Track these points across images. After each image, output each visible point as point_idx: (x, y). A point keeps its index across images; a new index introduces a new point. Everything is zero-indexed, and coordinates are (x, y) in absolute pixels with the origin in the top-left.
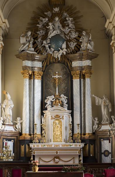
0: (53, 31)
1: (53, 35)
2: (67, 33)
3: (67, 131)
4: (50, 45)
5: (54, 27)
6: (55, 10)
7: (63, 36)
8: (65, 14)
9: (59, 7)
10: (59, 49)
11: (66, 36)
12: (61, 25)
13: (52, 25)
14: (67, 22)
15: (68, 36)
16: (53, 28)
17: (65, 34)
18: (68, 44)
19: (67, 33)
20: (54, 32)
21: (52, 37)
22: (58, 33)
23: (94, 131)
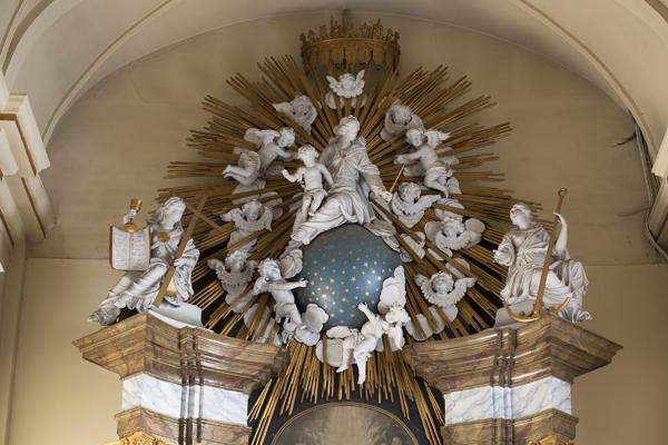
0: (324, 201)
1: (327, 227)
4: (302, 284)
6: (340, 93)
7: (385, 233)
8: (402, 112)
9: (361, 74)
10: (363, 308)
11: (408, 240)
12: (372, 171)
13: (322, 167)
14: (414, 156)
15: (417, 239)
17: (400, 229)
19: (409, 223)
20: (333, 204)
22: (354, 213)
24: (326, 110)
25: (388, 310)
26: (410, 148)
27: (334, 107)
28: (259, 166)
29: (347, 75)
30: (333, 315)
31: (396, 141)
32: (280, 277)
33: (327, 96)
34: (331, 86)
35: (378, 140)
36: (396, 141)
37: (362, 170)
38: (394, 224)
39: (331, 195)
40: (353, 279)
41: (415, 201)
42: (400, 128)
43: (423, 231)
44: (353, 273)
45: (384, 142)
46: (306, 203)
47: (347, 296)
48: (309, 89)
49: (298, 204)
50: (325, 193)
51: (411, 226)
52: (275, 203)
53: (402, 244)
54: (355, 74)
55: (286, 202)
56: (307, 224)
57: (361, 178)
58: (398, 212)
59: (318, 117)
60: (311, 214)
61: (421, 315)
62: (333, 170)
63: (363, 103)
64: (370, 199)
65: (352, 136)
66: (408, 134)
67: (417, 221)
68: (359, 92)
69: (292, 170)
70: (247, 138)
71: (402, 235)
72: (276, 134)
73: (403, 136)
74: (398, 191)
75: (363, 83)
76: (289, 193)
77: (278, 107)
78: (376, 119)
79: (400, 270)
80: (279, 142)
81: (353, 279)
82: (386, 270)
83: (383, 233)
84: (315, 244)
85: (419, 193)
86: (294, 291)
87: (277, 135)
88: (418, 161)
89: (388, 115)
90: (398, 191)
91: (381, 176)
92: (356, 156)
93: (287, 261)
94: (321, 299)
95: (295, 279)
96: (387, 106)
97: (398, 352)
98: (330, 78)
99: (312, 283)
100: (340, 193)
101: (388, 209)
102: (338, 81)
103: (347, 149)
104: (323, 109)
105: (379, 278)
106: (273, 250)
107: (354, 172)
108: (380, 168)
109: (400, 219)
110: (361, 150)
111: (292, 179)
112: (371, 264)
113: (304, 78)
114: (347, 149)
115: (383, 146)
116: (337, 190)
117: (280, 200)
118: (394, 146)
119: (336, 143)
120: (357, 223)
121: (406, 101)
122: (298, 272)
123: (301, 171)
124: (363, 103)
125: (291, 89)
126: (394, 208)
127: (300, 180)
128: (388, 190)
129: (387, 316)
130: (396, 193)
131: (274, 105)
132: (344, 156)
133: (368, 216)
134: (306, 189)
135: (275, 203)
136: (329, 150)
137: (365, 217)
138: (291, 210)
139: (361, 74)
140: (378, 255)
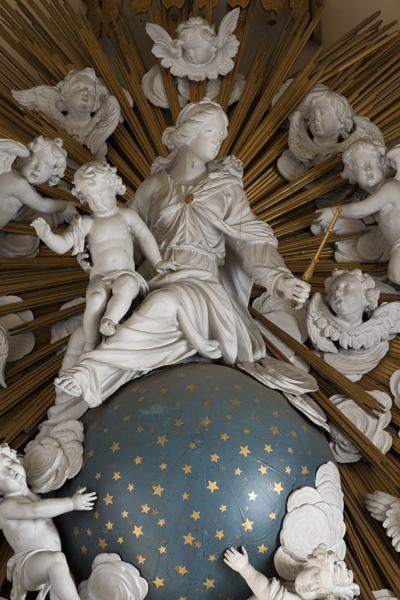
0: (138, 302)
1: (146, 364)
2: (352, 369)
3: (211, 231)
4: (83, 501)
5: (153, 251)
6: (179, 68)
7: (293, 385)
8: (330, 109)
9: (231, 20)
10: (239, 562)
11: (348, 409)
12: (258, 236)
13: (131, 218)
14: (361, 209)
15: (372, 408)
16: (141, 261)
17: (327, 385)
18: (378, 527)
19: (352, 369)
20: (163, 307)
21: (134, 389)
22: (213, 335)
23: (16, 299)
24: (145, 110)
25: (301, 568)
26: (358, 192)
27: (164, 104)
29: (196, 22)
30: (159, 582)
31: (317, 181)
32: (25, 491)
33: (147, 77)
34: (157, 51)
35: (271, 179)
36: (317, 181)
37: (233, 233)
38: (313, 371)
39: (153, 289)
40: (213, 486)
41: (366, 317)
42: (325, 147)
43: (387, 389)
44: (212, 472)
45: (285, 182)
46: (95, 302)
47: (195, 528)
48: (97, 52)
49: (72, 323)
50: (144, 284)
51: (358, 378)
52: (15, 320)
53: (333, 417)
54: (215, 22)
55: (41, 320)
56: (97, 355)
57: (231, 260)
58: (323, 344)
59: (125, 125)
60: (106, 329)
61: (385, 592)
62: (163, 233)
63: (236, 95)
64: (255, 315)
65: (211, 150)
66: (347, 158)
67: (372, 366)
68: (226, 65)
69: (61, 227)
71: (334, 399)
72: (19, 149)
73: (336, 165)
74: (321, 284)
75: (235, 44)
76: (51, 298)
77: (25, 98)
78: (266, 129)
79: (328, 474)
80: (28, 172)
81: (213, 486)
82: (297, 469)
83: (287, 384)
84: (116, 406)
85: (375, 296)
86: (60, 523)
87: (24, 152)
88: (372, 223)
89: (296, 118)
90: (321, 284)
91: (279, 250)
92: (219, 199)
93: (40, 448)
94: (128, 535)
95: (66, 490)
96: (295, 100)
97: (392, 451)
98: (154, 30)
99: (108, 500)
100: (180, 283)
101: (298, 337)
102: (175, 36)
103: (198, 182)
104: (135, 108)
105: (278, 488)
106: (12, 429)
107: (215, 239)
109: (328, 359)
110: (230, 181)
111: (59, 244)
112: (257, 451)
113: (88, 35)
114: (195, 183)
115: (286, 191)
116: (167, 279)
117: (29, 316)
118: (313, 192)
119: (169, 169)
120: (220, 362)
121: (349, 88)
122: (69, 474)
123: (83, 226)
124: (236, 95)
125: (56, 58)
126: (314, 333)
127: (79, 249)
128: (298, 274)
129: (301, 582)
132: (189, 198)
133: (249, 349)
134: (94, 272)
135: (15, 320)
136: (151, 187)
137: (241, 349)
138: (55, 338)
139: (231, 20)
140: (275, 431)
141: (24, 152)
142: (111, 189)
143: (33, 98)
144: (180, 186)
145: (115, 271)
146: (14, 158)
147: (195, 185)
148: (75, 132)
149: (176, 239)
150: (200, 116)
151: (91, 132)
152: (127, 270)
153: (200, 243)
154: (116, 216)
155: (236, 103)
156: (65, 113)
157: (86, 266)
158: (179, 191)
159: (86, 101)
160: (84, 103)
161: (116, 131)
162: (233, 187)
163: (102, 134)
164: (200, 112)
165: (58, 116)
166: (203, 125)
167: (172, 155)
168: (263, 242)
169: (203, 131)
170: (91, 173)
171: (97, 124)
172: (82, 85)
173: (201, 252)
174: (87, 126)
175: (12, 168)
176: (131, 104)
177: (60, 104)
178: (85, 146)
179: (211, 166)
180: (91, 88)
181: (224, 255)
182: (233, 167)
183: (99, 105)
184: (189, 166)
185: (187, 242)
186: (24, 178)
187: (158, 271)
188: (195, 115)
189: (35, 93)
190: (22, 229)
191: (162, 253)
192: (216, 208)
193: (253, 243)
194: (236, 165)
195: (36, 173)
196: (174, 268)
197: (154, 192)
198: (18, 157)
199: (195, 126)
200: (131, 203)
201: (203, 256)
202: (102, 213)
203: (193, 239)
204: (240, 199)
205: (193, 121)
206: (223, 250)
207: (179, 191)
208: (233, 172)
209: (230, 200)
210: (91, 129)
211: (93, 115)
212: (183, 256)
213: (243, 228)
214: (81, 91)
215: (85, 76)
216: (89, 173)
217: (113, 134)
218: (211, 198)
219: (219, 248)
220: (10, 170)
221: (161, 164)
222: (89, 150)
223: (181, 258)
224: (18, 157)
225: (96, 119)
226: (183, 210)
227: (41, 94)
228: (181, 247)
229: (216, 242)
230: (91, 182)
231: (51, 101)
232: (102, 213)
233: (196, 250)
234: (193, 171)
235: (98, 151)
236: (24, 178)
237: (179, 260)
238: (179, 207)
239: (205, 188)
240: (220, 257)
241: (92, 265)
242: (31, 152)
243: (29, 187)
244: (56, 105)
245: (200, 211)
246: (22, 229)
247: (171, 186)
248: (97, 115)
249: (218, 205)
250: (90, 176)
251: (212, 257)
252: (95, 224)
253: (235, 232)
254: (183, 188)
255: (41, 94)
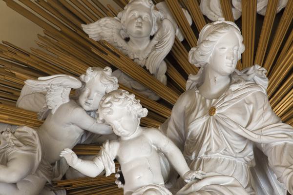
28: (38, 157)
37: (255, 138)
65: (227, 64)
70: (24, 102)
77: (94, 30)
80: (82, 100)
87: (77, 84)
92: (240, 109)
107: (241, 145)
108: (86, 70)
111: (89, 169)
114: (217, 97)
123: (110, 150)
130: (195, 181)
131: (85, 27)
132: (212, 111)
141: (76, 84)
142: (130, 114)
143: (99, 30)
144: (205, 99)
145: (141, 187)
146: (70, 90)
147: (218, 98)
148: (136, 56)
149: (204, 149)
150: (213, 36)
151: (150, 53)
152: (152, 185)
153: (225, 150)
154: (139, 137)
155: (283, 10)
156: (127, 40)
157: (119, 184)
158: (204, 105)
159: (141, 27)
160: (139, 29)
161: (173, 47)
162: (254, 95)
163: (158, 55)
164: (213, 33)
165: (121, 43)
166: (217, 43)
167: (200, 71)
168: (282, 143)
169: (217, 49)
170: (109, 102)
171: (155, 46)
172: (136, 14)
173: (227, 158)
174: (145, 50)
175: (70, 99)
176: (190, 23)
177: (122, 32)
178: (145, 67)
179: (232, 78)
180: (145, 15)
181: (253, 157)
182: (258, 75)
183: (157, 29)
184: (212, 81)
185: (213, 151)
186: (81, 106)
187: (186, 181)
188: (208, 36)
189: (99, 25)
190: (90, 151)
191: (190, 163)
192: (236, 117)
193: (274, 145)
194: (260, 73)
195: (89, 101)
196: (199, 177)
197: (185, 107)
198: (72, 89)
199: (210, 45)
200: (170, 119)
201: (229, 161)
202: (127, 136)
203: (219, 148)
204: (260, 105)
205: (208, 40)
206: (252, 153)
207: (204, 105)
208: (258, 79)
209: (251, 107)
210: (150, 51)
211: (152, 38)
212: (211, 163)
213: (264, 132)
214: (136, 19)
215: (140, 4)
216: (107, 103)
217: (171, 51)
218: (233, 108)
219: (245, 152)
220: (67, 100)
221: (193, 81)
222: (148, 71)
223: (208, 167)
224: (72, 89)
225: (155, 41)
226: (208, 122)
227: (105, 26)
228: (209, 156)
229: (243, 147)
230: (108, 110)
231: (114, 31)
232: (127, 136)
233: (223, 157)
234: (217, 84)
235: (158, 70)
236: (81, 106)
237: (206, 169)
238: (205, 119)
239: (226, 100)
240: (248, 160)
241: (123, 182)
242: (84, 83)
243: (85, 113)
244: (119, 34)
245: (222, 122)
246: (90, 151)
247: (198, 101)
248: (155, 38)
249: (238, 114)
250: (108, 105)
251: (240, 162)
252: (121, 146)
253: (257, 136)
254: (208, 102)
255: (105, 26)
